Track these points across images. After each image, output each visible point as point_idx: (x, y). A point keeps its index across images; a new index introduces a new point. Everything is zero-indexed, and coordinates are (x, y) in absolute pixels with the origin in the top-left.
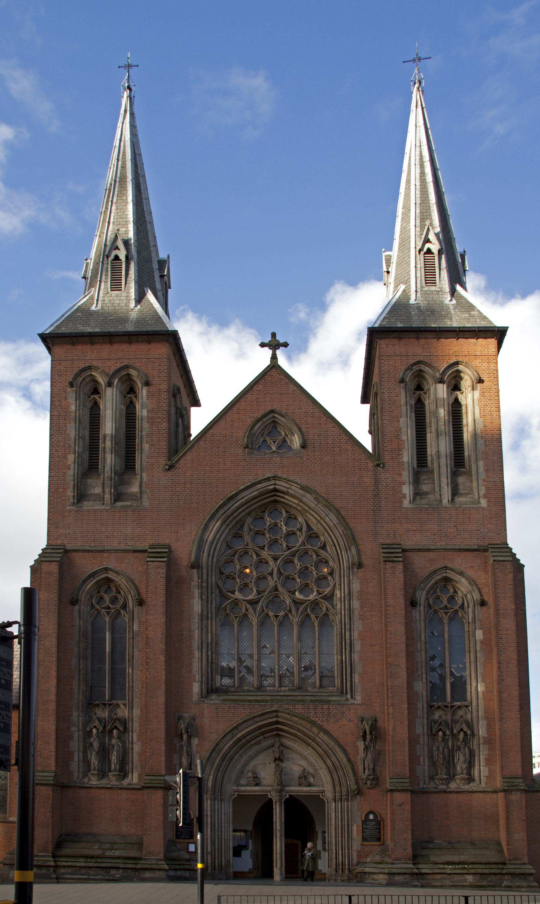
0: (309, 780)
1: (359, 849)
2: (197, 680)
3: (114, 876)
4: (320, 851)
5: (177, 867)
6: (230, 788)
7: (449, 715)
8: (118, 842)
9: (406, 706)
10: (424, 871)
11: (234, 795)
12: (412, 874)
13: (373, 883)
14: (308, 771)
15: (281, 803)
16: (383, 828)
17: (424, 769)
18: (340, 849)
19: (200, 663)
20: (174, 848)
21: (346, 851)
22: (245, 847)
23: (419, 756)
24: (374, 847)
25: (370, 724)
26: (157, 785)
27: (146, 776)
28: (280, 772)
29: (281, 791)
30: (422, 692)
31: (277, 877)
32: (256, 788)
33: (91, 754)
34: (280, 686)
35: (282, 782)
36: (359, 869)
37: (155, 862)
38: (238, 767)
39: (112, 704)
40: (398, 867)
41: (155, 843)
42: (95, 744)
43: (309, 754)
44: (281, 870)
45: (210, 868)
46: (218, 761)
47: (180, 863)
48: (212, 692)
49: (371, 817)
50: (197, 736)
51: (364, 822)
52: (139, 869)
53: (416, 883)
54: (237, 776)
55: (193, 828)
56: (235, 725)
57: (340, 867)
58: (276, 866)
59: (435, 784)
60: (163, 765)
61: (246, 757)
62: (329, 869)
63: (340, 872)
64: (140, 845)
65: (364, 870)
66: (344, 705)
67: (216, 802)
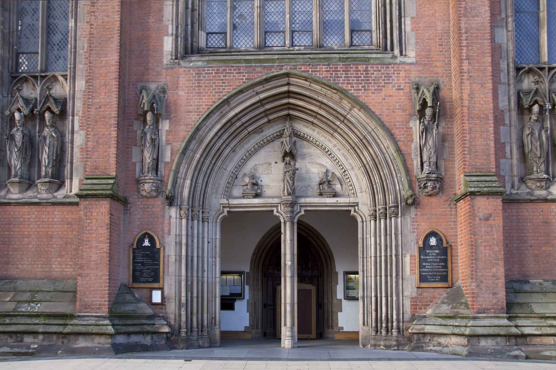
0: (334, 187)
1: (414, 295)
2: (170, 32)
3: (28, 347)
4: (341, 300)
5: (131, 329)
6: (217, 202)
7: (547, 81)
8: (43, 289)
9: (489, 59)
10: (527, 331)
11: (223, 212)
12: (508, 336)
13: (440, 352)
14: (333, 173)
15: (292, 223)
16: (452, 260)
17: (512, 165)
18: (383, 295)
19: (175, 7)
20: (128, 297)
21: (394, 298)
22: (240, 296)
23: (504, 143)
24: (437, 290)
25: (432, 91)
26: (101, 192)
27: (87, 179)
28: (293, 176)
29: (293, 204)
30: (507, 45)
31: (286, 341)
32: (256, 201)
33: (11, 152)
34: (292, 45)
35: (294, 189)
36: (414, 328)
37: (94, 322)
38: (229, 168)
39: (46, 76)
40: (485, 324)
41: (96, 289)
42: (17, 136)
43: (335, 146)
44: (292, 332)
45: (184, 330)
46: (198, 156)
47: (136, 322)
48: (192, 52)
49: (433, 241)
50: (168, 117)
51: (422, 250)
52: (69, 334)
53: (517, 353)
54: (228, 183)
55: (159, 265)
56: (225, 97)
57: (384, 325)
58: (285, 325)
59: (528, 187)
60: (113, 160)
61: (241, 153)
62: (365, 328)
63: (384, 333)
64: (72, 294)
65: (423, 329)
66: (390, 64)
67: (196, 222)
